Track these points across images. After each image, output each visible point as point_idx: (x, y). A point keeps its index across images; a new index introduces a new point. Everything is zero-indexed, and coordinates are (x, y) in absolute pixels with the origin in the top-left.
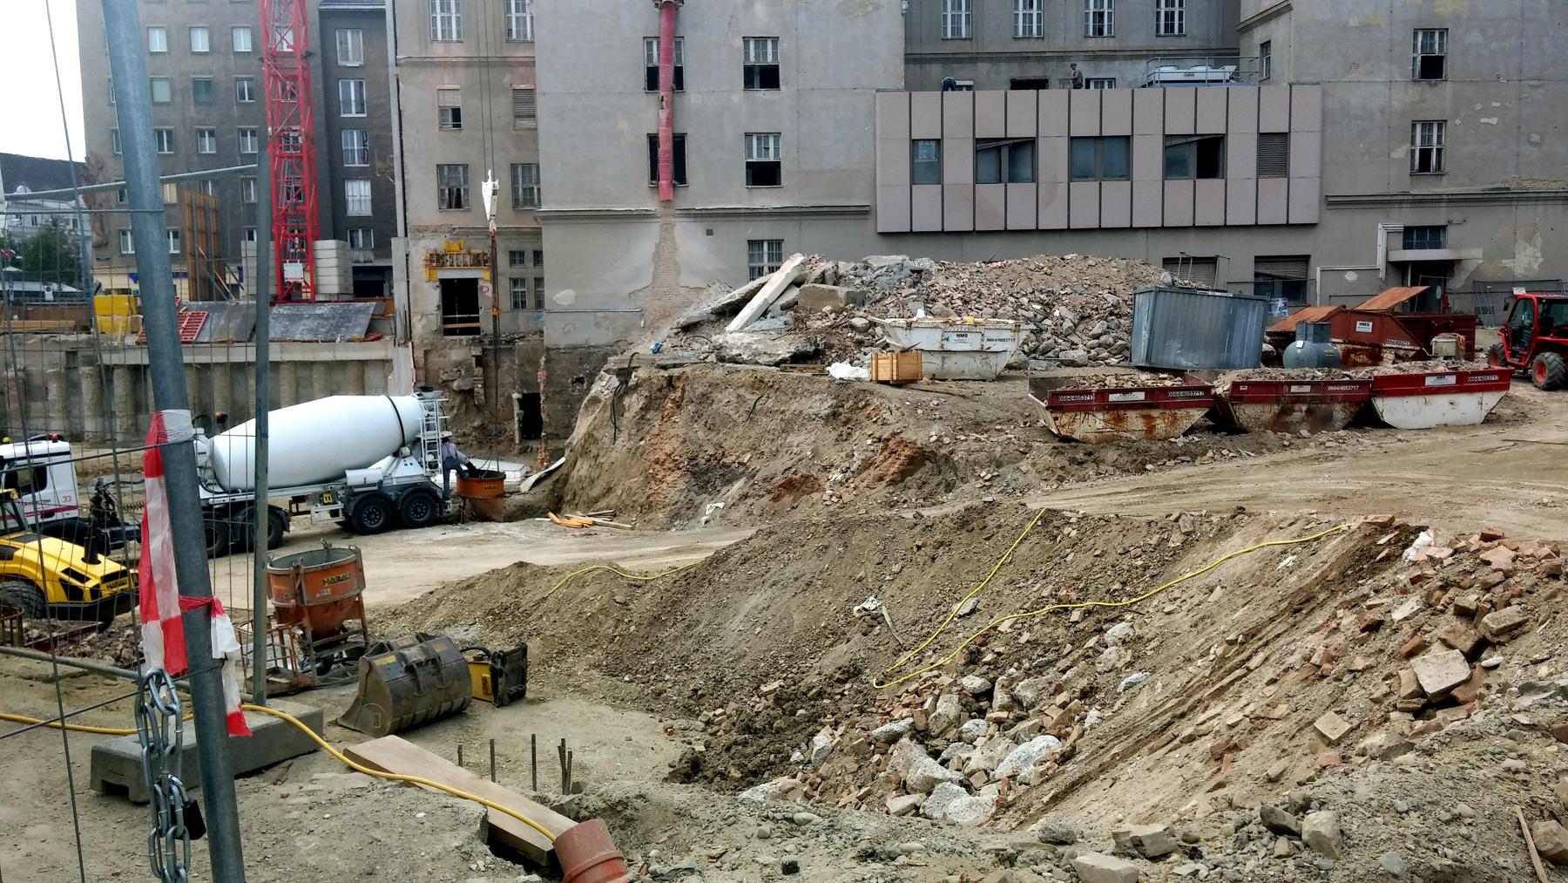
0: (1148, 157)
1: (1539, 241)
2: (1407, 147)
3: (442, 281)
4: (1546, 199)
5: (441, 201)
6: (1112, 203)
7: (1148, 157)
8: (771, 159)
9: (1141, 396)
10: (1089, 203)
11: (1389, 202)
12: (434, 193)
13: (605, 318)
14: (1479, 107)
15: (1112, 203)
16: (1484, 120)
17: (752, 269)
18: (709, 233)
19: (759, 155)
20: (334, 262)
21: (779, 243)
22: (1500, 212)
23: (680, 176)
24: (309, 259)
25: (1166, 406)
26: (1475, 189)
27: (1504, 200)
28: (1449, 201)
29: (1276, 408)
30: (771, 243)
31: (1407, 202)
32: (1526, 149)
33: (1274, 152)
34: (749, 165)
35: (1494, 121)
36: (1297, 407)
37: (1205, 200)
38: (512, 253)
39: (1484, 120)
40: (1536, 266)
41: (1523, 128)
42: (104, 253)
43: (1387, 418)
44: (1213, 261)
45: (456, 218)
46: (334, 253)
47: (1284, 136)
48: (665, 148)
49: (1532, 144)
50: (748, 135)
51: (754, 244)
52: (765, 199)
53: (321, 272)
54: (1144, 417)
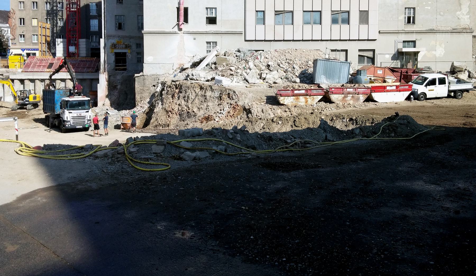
0: (327, 18)
1: (443, 46)
2: (404, 16)
3: (115, 53)
4: (445, 32)
5: (116, 27)
6: (316, 32)
7: (327, 18)
8: (214, 16)
9: (303, 92)
10: (310, 32)
11: (398, 33)
12: (114, 24)
13: (163, 66)
14: (424, 3)
15: (316, 32)
16: (426, 8)
17: (207, 51)
18: (195, 39)
19: (210, 14)
20: (85, 46)
21: (216, 43)
22: (431, 35)
23: (186, 20)
24: (77, 46)
25: (310, 96)
26: (424, 29)
27: (433, 32)
28: (416, 33)
29: (343, 95)
30: (213, 42)
31: (403, 33)
32: (439, 17)
33: (364, 17)
34: (207, 18)
35: (429, 8)
36: (349, 95)
37: (342, 31)
38: (137, 44)
39: (426, 8)
40: (443, 54)
41: (438, 10)
42: (14, 42)
43: (375, 99)
44: (414, 42)
45: (120, 33)
46: (85, 43)
47: (367, 12)
48: (182, 12)
49: (441, 15)
50: (207, 8)
51: (208, 43)
52: (212, 28)
53: (81, 49)
54: (305, 98)
